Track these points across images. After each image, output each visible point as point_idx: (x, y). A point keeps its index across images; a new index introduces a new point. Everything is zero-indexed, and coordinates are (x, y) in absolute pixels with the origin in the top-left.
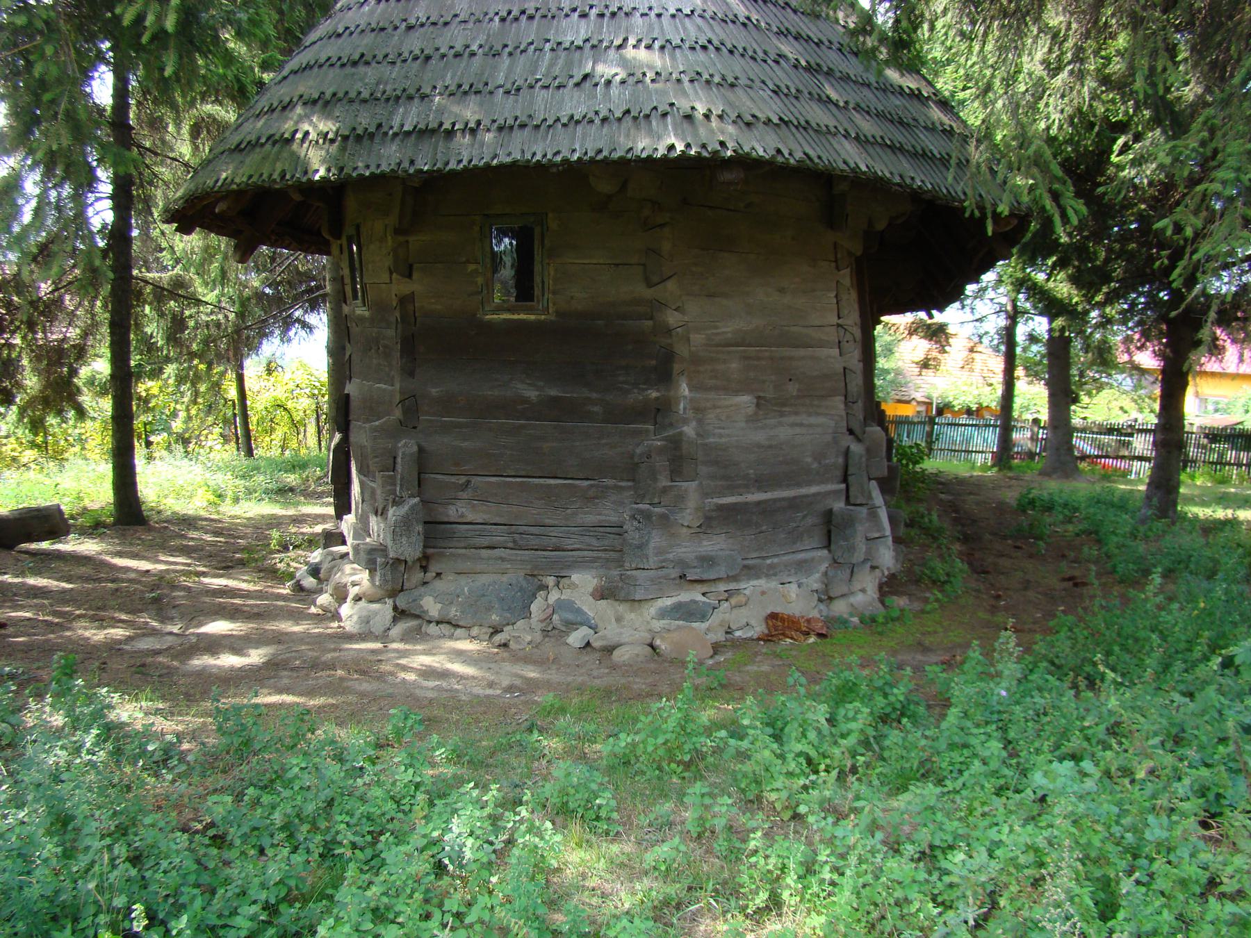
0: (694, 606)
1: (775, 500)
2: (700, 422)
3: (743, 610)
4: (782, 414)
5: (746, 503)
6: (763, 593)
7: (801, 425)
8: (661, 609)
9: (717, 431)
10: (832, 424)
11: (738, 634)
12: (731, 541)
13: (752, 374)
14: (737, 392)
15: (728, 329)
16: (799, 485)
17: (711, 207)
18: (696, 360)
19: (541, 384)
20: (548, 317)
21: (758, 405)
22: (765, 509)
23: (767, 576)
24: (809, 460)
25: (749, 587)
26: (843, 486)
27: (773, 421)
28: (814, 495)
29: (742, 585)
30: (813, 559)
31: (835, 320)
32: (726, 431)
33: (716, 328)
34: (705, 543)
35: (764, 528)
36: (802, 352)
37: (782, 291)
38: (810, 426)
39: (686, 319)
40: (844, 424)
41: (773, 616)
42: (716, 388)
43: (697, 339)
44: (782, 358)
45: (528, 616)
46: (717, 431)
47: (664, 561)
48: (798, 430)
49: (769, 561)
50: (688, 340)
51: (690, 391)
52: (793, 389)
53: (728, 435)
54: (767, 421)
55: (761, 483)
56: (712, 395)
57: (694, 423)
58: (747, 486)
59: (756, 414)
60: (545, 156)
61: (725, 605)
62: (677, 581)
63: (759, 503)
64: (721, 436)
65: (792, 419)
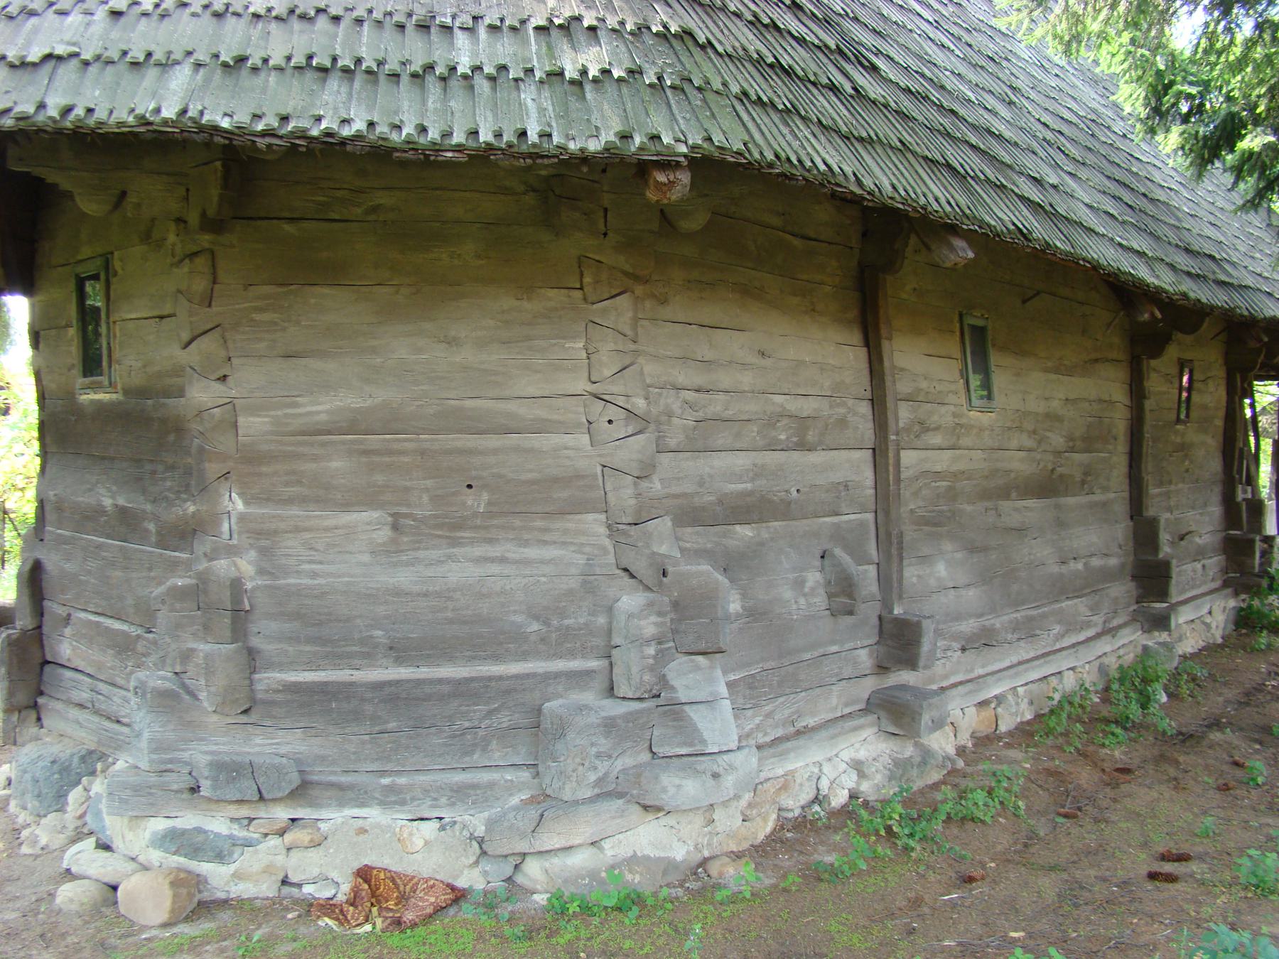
0: (201, 838)
1: (419, 683)
2: (265, 552)
3: (313, 855)
4: (455, 542)
5: (352, 684)
6: (362, 831)
7: (503, 560)
8: (154, 834)
9: (306, 567)
10: (581, 559)
11: (308, 889)
12: (318, 741)
13: (379, 478)
14: (346, 506)
15: (320, 408)
16: (496, 658)
17: (292, 219)
18: (252, 458)
19: (114, 488)
20: (114, 396)
21: (395, 527)
22: (391, 695)
23: (383, 804)
24: (519, 618)
25: (333, 817)
26: (605, 663)
27: (434, 554)
28: (517, 677)
29: (324, 814)
30: (491, 785)
31: (582, 385)
32: (332, 568)
33: (296, 405)
34: (258, 740)
35: (392, 725)
36: (493, 441)
37: (451, 342)
38: (526, 562)
39: (233, 393)
40: (611, 559)
41: (364, 874)
42: (303, 501)
43: (253, 425)
44: (449, 452)
45: (61, 810)
46: (306, 567)
47: (171, 761)
48: (495, 569)
49: (386, 781)
50: (235, 425)
51: (246, 503)
52: (477, 502)
53: (330, 575)
54: (421, 554)
55: (399, 652)
56: (295, 511)
57: (253, 554)
58: (367, 655)
59: (393, 541)
60: (498, 135)
61: (274, 841)
62: (186, 795)
63: (379, 686)
64: (314, 575)
65: (478, 551)
